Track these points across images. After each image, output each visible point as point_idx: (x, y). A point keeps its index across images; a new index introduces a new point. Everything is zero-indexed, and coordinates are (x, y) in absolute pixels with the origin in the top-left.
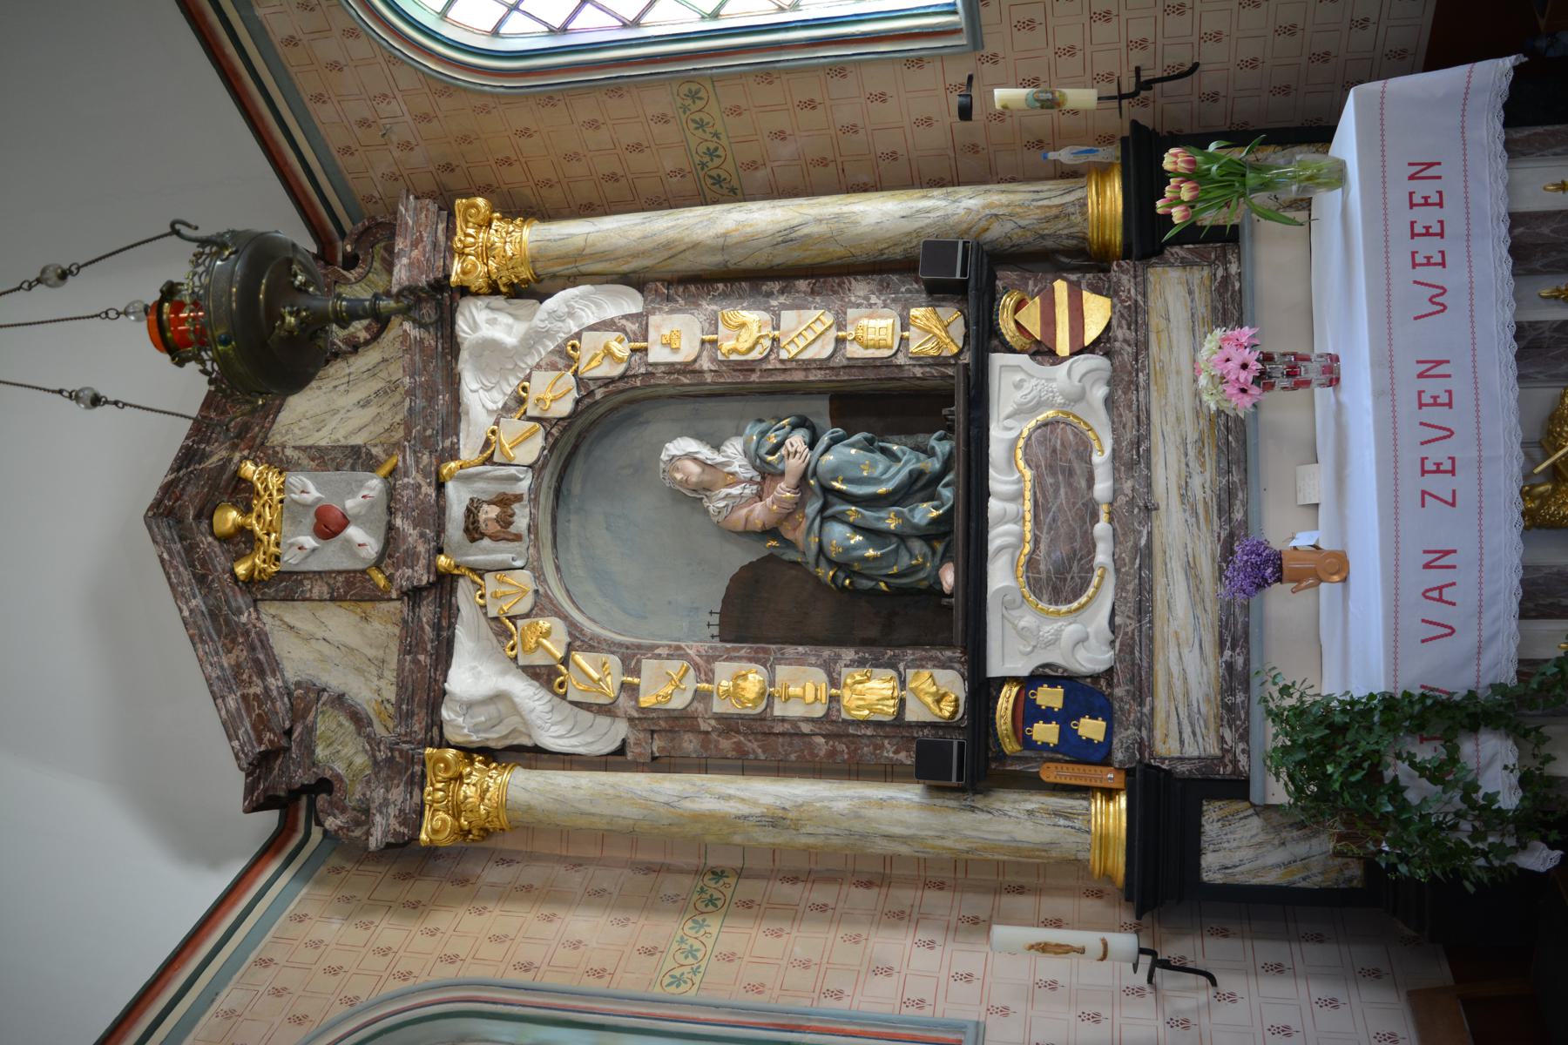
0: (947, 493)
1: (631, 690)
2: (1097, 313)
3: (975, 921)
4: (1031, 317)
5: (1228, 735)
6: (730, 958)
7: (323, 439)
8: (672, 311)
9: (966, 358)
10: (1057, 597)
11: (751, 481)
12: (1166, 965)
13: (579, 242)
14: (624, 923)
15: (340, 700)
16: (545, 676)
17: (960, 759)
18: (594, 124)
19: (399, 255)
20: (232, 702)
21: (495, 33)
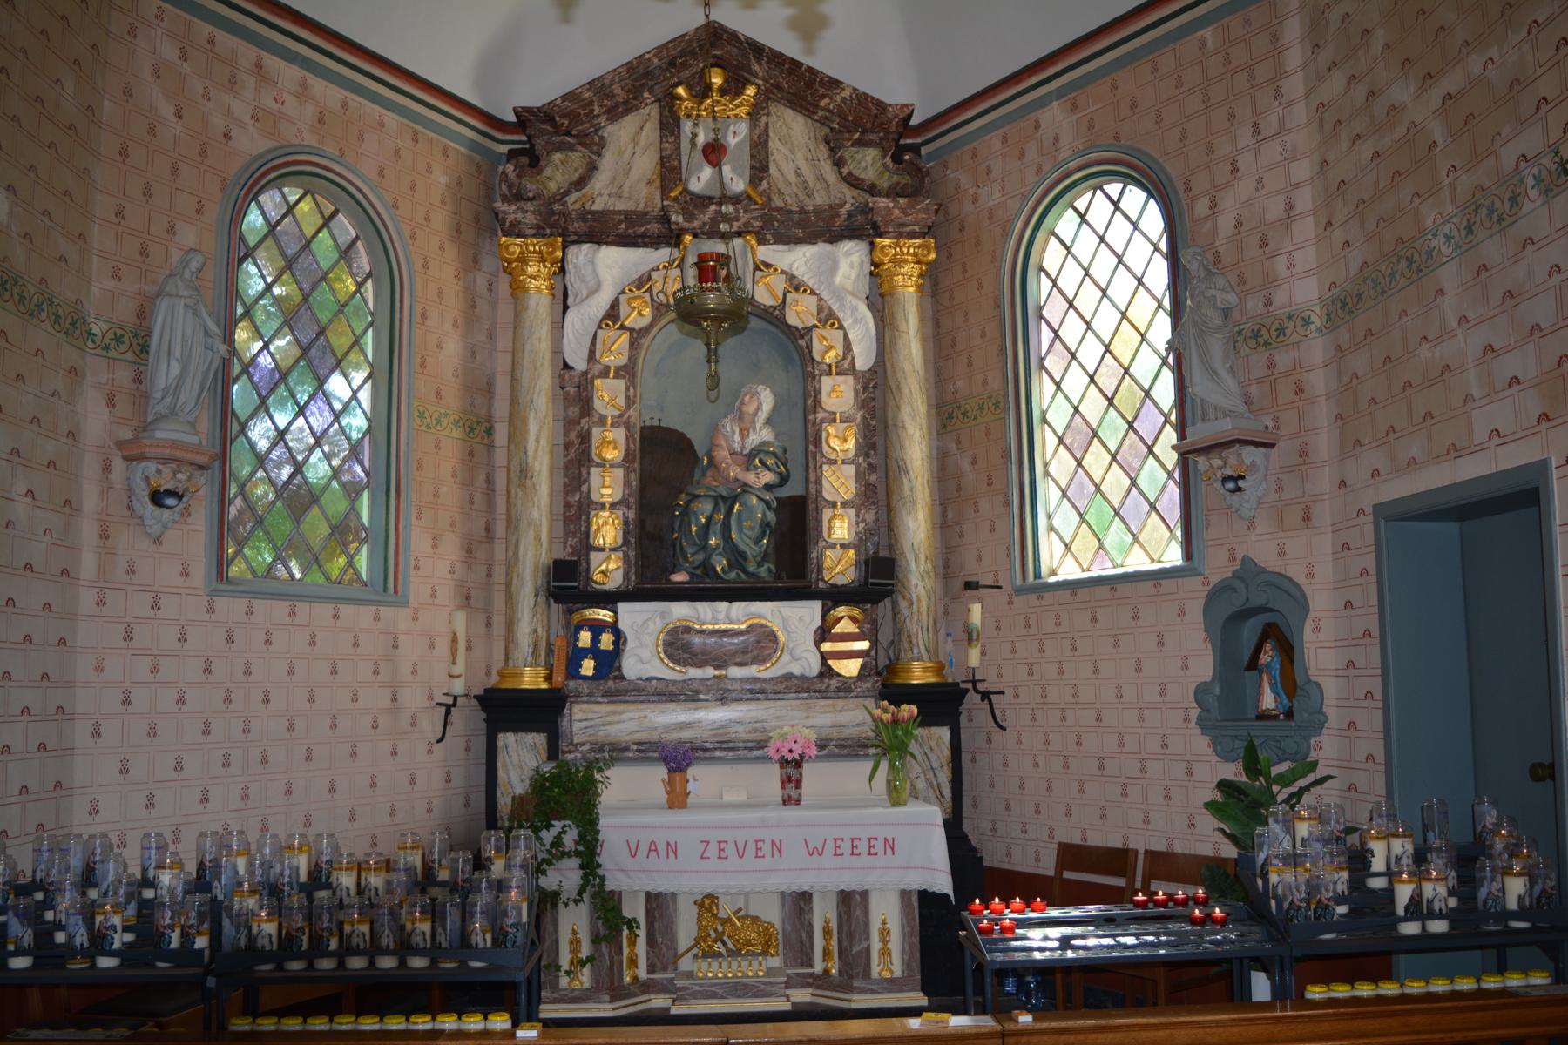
0: (733, 575)
1: (605, 373)
2: (850, 668)
3: (468, 598)
4: (845, 626)
5: (585, 748)
6: (438, 447)
7: (774, 144)
8: (856, 392)
9: (822, 585)
10: (668, 645)
11: (743, 447)
12: (448, 713)
13: (902, 327)
14: (455, 375)
15: (592, 168)
16: (612, 314)
17: (568, 584)
18: (983, 335)
19: (894, 201)
20: (586, 95)
21: (1042, 269)
